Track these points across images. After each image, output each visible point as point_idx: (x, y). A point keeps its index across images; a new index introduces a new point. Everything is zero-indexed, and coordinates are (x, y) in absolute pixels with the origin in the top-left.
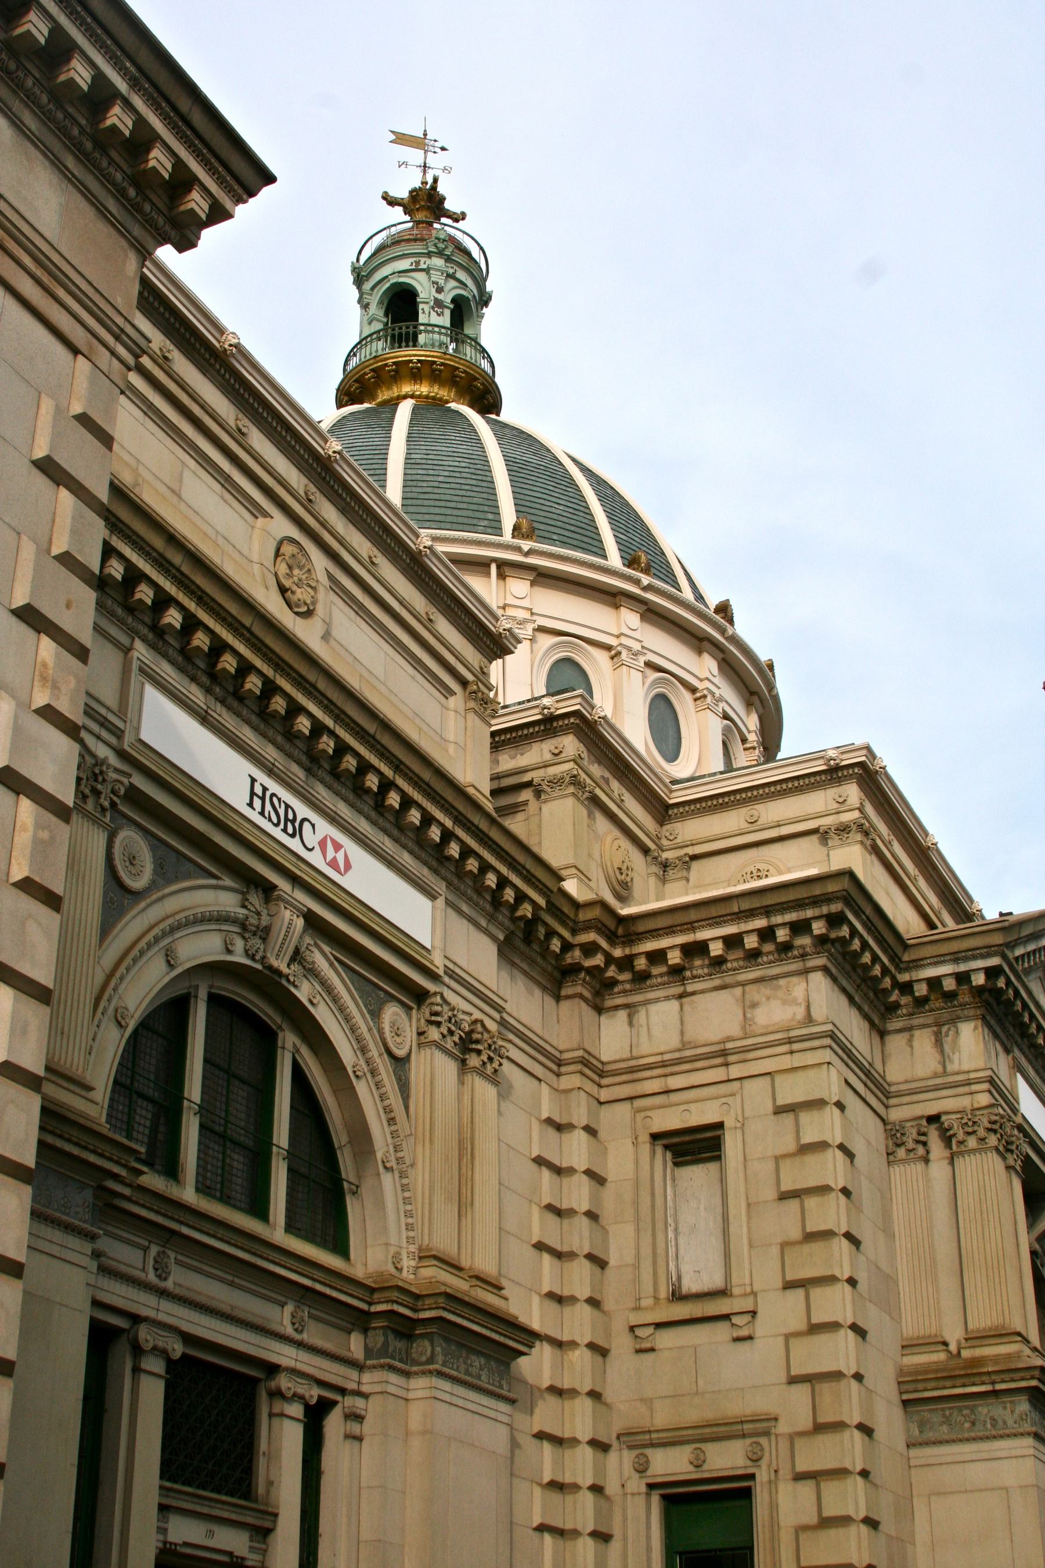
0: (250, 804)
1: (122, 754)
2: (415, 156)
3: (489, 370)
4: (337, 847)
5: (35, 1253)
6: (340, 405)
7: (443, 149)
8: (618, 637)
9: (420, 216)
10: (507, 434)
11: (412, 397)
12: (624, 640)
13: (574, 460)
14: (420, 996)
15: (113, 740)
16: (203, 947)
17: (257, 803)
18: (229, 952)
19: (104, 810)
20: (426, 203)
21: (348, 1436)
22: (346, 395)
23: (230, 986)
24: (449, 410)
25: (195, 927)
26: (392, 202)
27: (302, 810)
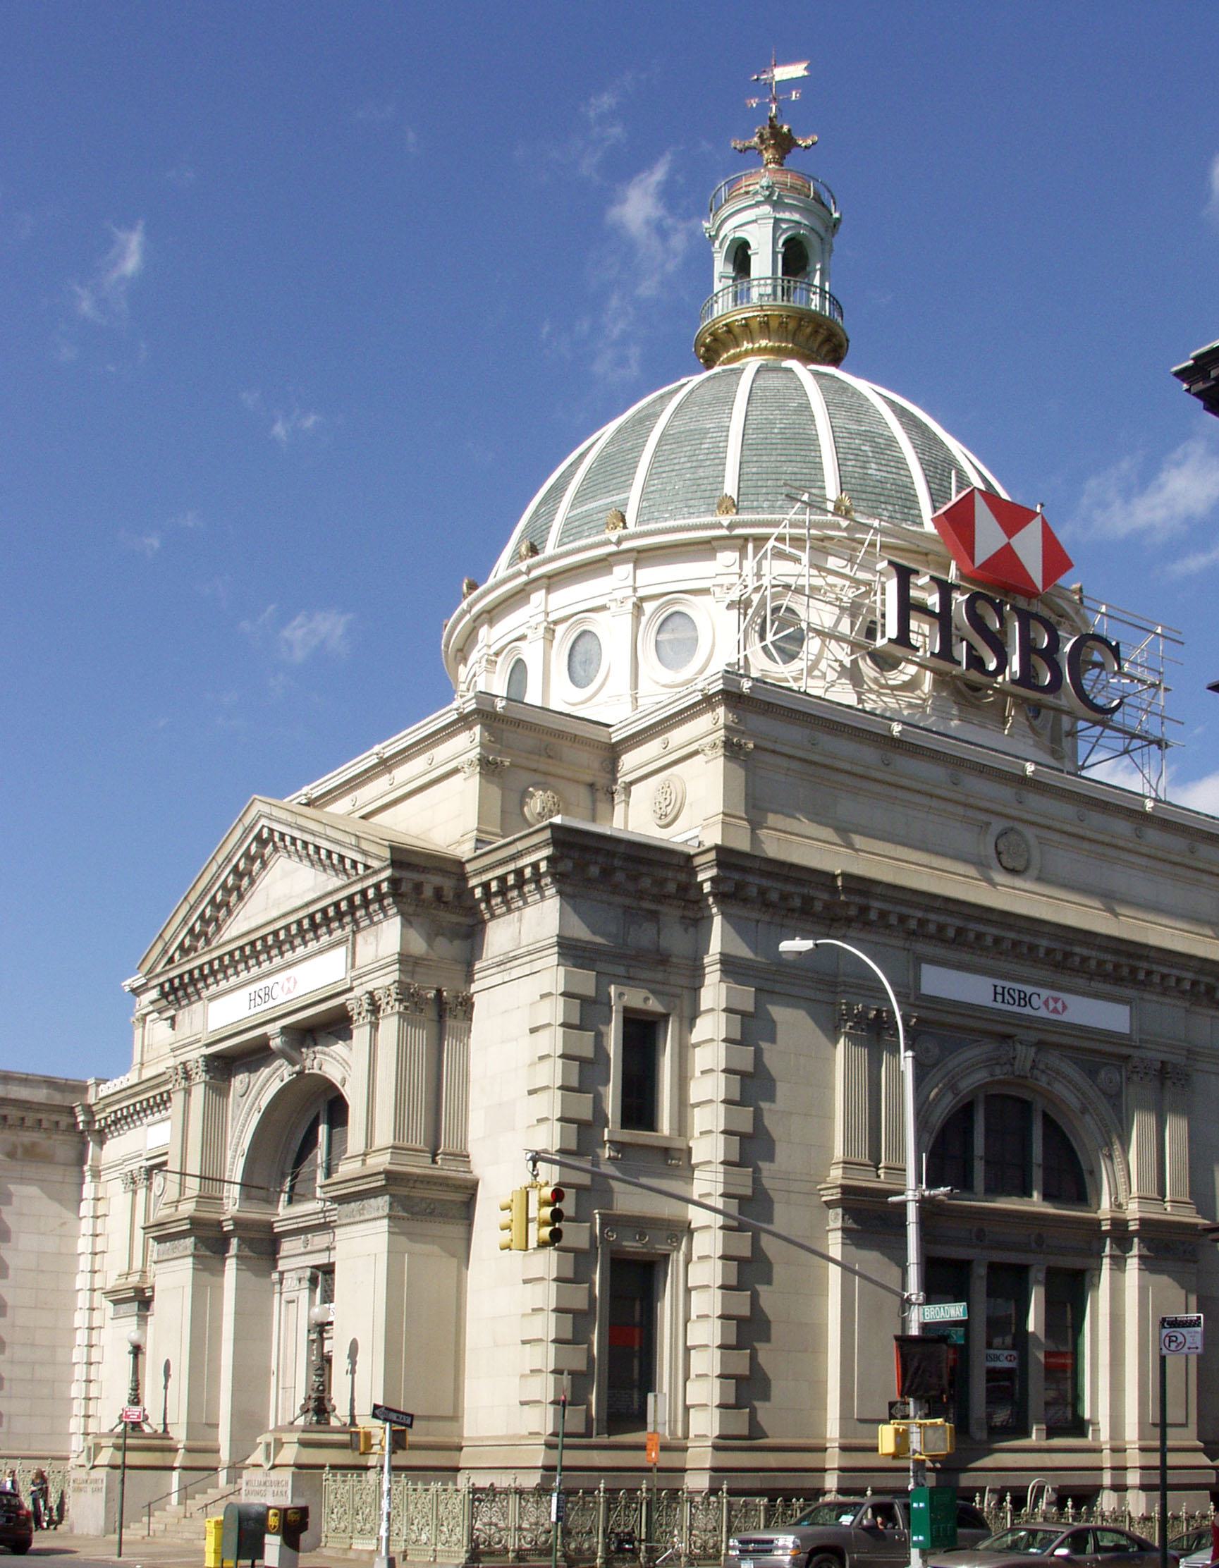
0: (995, 1000)
4: (1056, 1000)
5: (458, 1151)
16: (980, 1076)
17: (999, 998)
21: (15, 1147)
27: (1029, 989)
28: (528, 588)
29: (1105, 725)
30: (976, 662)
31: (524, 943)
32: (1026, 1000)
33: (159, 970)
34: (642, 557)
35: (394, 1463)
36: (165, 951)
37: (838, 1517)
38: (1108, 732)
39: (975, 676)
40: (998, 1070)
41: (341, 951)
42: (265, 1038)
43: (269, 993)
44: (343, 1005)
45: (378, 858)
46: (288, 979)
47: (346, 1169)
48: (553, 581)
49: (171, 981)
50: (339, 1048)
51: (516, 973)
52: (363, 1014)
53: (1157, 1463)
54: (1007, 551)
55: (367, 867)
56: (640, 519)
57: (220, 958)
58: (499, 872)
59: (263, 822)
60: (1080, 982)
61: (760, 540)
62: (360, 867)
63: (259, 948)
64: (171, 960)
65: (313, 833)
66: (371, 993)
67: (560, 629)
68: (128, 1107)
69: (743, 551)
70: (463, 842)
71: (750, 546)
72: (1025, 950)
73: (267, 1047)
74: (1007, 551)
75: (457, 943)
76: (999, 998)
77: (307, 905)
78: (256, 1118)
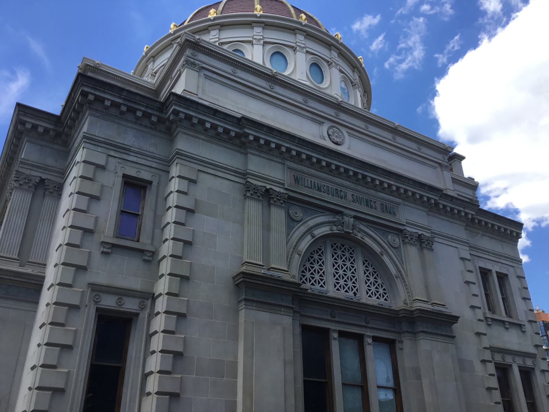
1: (286, 189)
8: (296, 43)
12: (298, 44)
14: (401, 231)
19: (282, 203)
23: (297, 233)
40: (335, 228)
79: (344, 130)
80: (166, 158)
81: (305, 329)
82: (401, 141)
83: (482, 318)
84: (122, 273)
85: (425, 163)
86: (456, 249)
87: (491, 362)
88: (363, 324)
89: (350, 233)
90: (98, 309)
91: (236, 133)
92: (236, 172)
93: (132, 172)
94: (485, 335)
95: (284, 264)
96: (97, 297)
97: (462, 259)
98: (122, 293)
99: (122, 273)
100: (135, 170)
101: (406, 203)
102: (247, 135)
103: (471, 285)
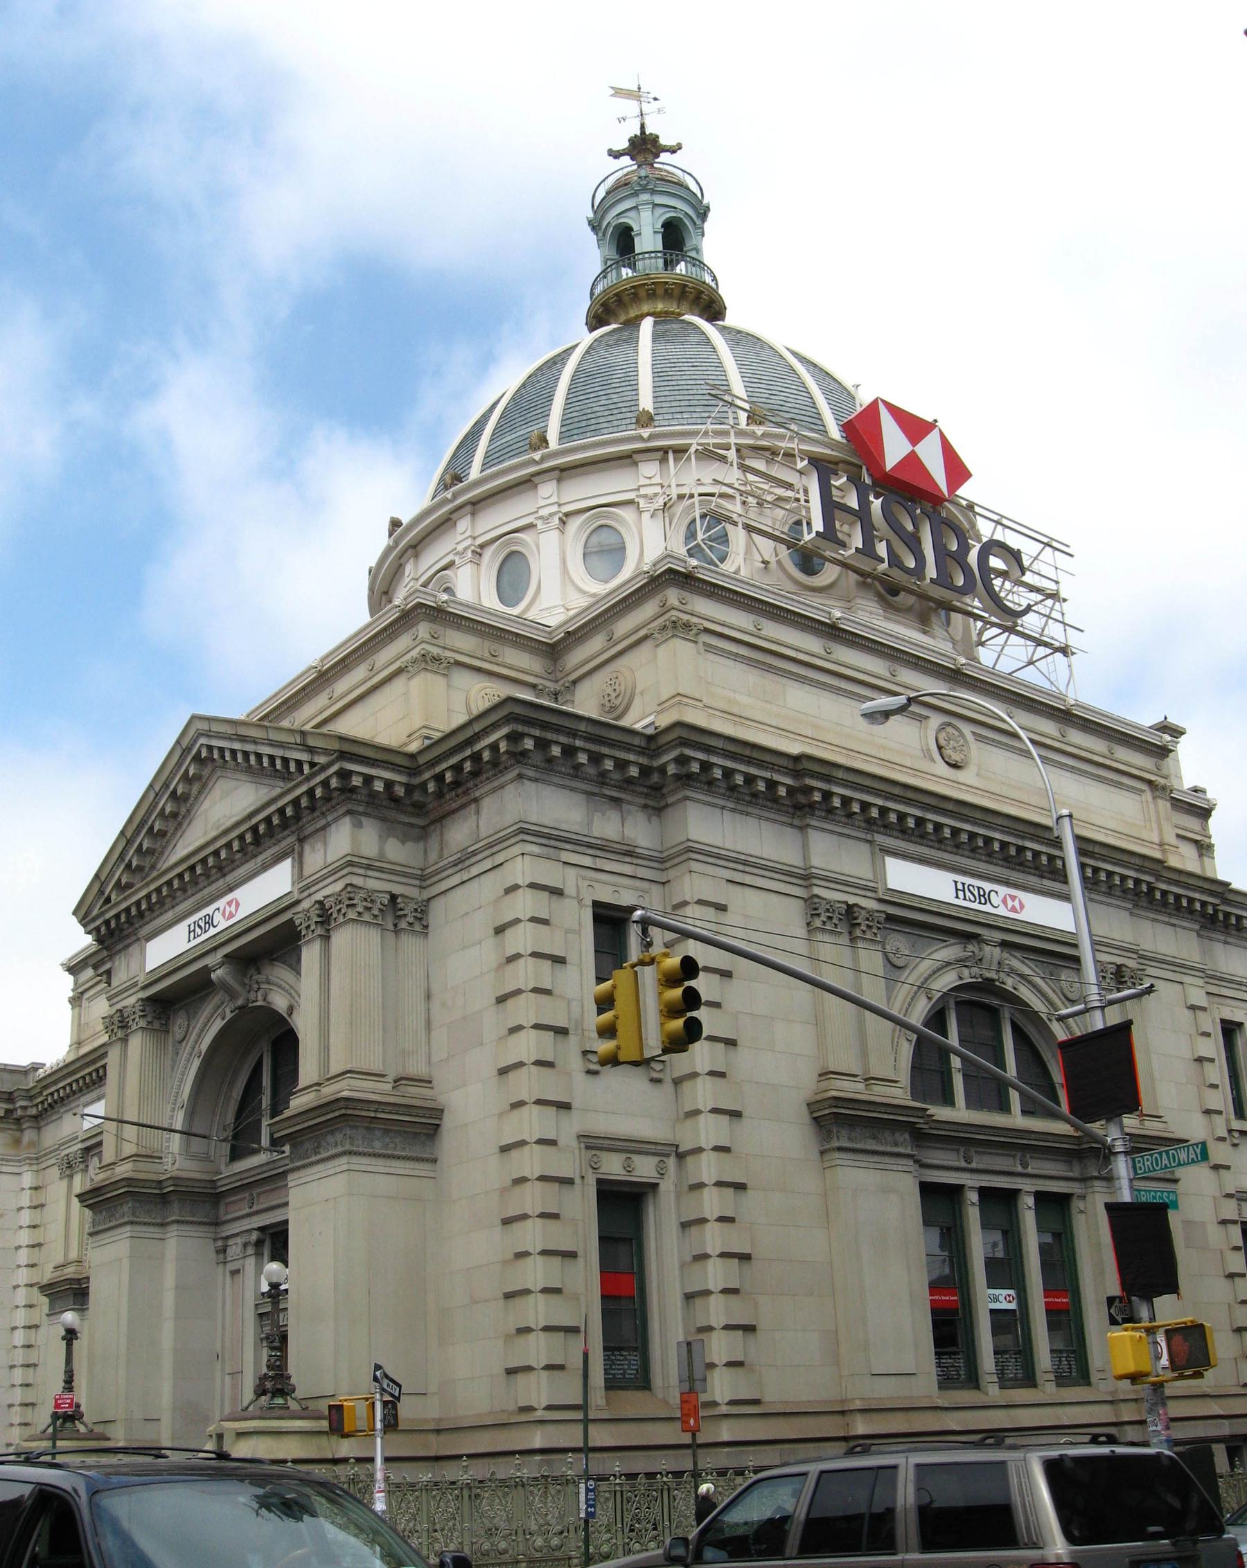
2: (631, 107)
3: (714, 286)
4: (1013, 898)
6: (592, 329)
7: (655, 99)
9: (640, 158)
10: (738, 338)
11: (649, 314)
13: (794, 354)
15: (873, 895)
16: (947, 981)
17: (961, 894)
18: (961, 978)
20: (644, 147)
22: (596, 320)
24: (684, 322)
25: (938, 970)
26: (616, 155)
27: (988, 886)
28: (454, 516)
29: (1012, 630)
30: (895, 561)
31: (483, 835)
32: (985, 897)
33: (95, 912)
34: (564, 473)
35: (387, 1455)
36: (101, 892)
37: (697, 1488)
38: (1014, 639)
39: (897, 574)
40: (966, 972)
41: (287, 864)
42: (207, 970)
43: (209, 921)
44: (291, 921)
45: (326, 751)
46: (229, 903)
47: (298, 1103)
48: (476, 506)
49: (107, 922)
50: (280, 973)
51: (475, 871)
52: (313, 927)
53: (592, 1429)
54: (912, 461)
55: (312, 765)
56: (563, 437)
57: (158, 890)
58: (453, 761)
59: (203, 741)
60: (1033, 880)
61: (680, 451)
62: (306, 768)
63: (199, 872)
64: (108, 900)
65: (255, 741)
66: (320, 903)
67: (488, 553)
68: (64, 1088)
69: (663, 461)
70: (411, 742)
71: (671, 456)
72: (981, 844)
73: (210, 983)
74: (912, 461)
75: (409, 845)
76: (961, 894)
77: (250, 816)
78: (197, 1063)
79: (967, 729)
80: (656, 854)
81: (927, 1190)
82: (1077, 738)
83: (1225, 1134)
84: (626, 1107)
85: (1121, 783)
86: (1180, 986)
87: (1235, 1222)
88: (1019, 1169)
89: (993, 980)
90: (599, 1181)
91: (788, 787)
92: (788, 874)
93: (606, 896)
94: (1228, 1168)
95: (888, 1070)
96: (595, 1159)
97: (1193, 1008)
98: (630, 1147)
99: (626, 1107)
100: (610, 889)
101: (1093, 896)
102: (810, 790)
103: (1206, 1064)
